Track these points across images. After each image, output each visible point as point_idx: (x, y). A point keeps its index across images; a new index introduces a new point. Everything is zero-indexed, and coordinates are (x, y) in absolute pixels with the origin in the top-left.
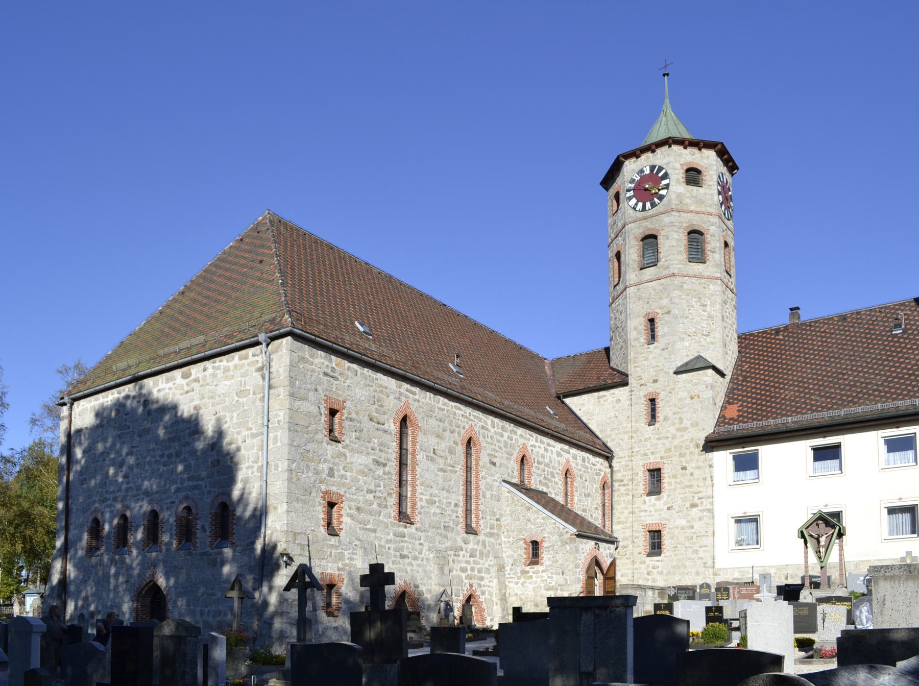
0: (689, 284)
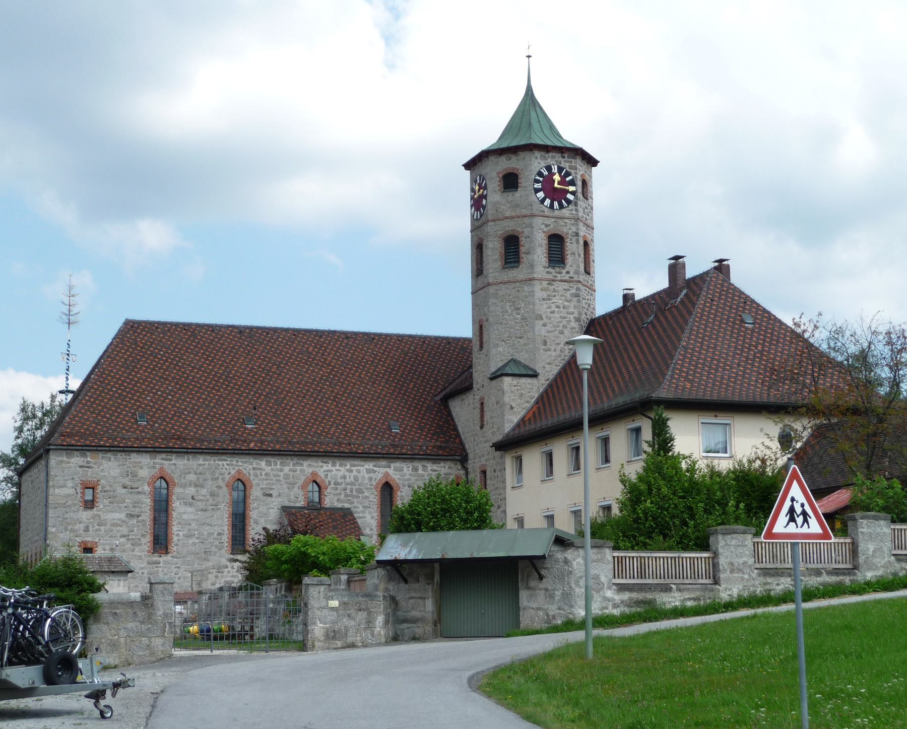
0: (504, 290)
